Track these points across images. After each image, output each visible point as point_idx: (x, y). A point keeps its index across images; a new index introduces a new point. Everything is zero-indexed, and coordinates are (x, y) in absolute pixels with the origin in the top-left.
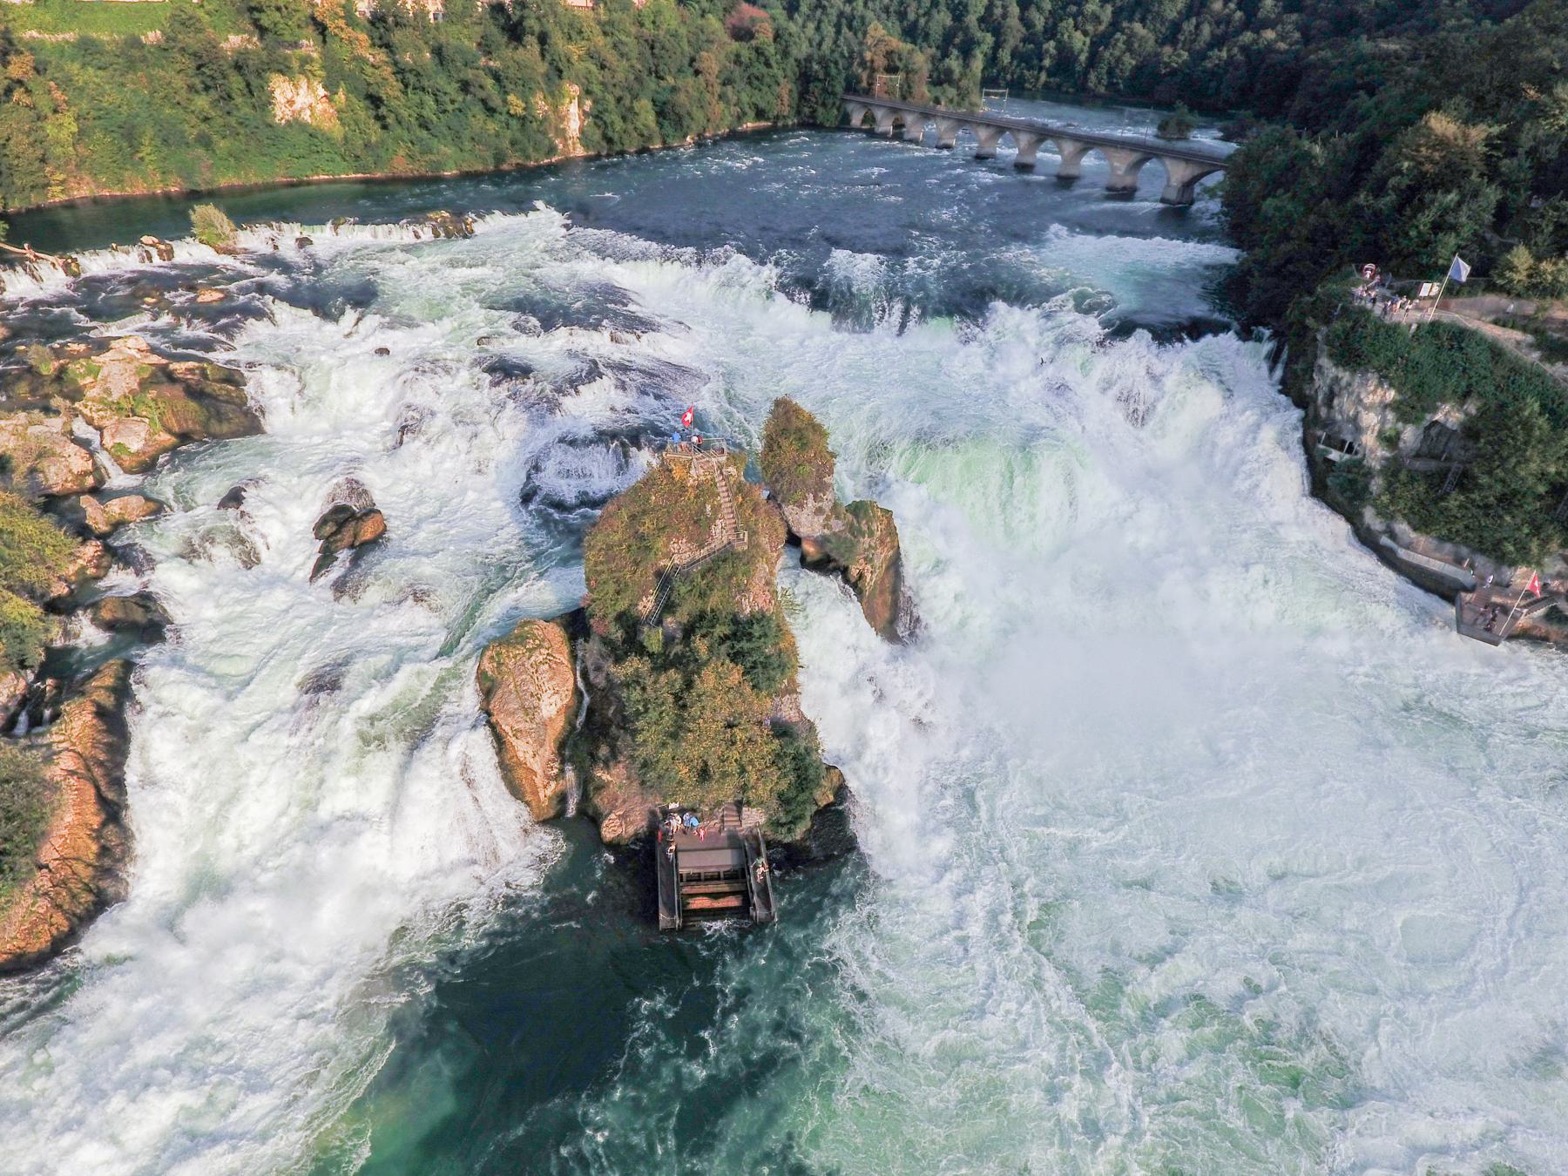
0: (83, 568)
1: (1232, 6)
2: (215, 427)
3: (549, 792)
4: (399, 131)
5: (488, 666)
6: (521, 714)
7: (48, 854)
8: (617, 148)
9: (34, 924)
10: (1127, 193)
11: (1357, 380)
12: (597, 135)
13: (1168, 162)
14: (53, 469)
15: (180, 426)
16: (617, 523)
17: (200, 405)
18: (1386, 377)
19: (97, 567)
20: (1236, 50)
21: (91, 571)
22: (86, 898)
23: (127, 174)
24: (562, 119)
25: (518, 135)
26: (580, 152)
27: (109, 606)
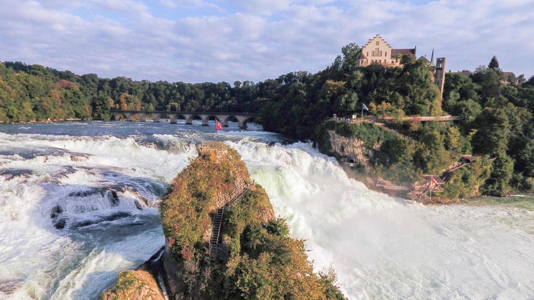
18: (360, 137)
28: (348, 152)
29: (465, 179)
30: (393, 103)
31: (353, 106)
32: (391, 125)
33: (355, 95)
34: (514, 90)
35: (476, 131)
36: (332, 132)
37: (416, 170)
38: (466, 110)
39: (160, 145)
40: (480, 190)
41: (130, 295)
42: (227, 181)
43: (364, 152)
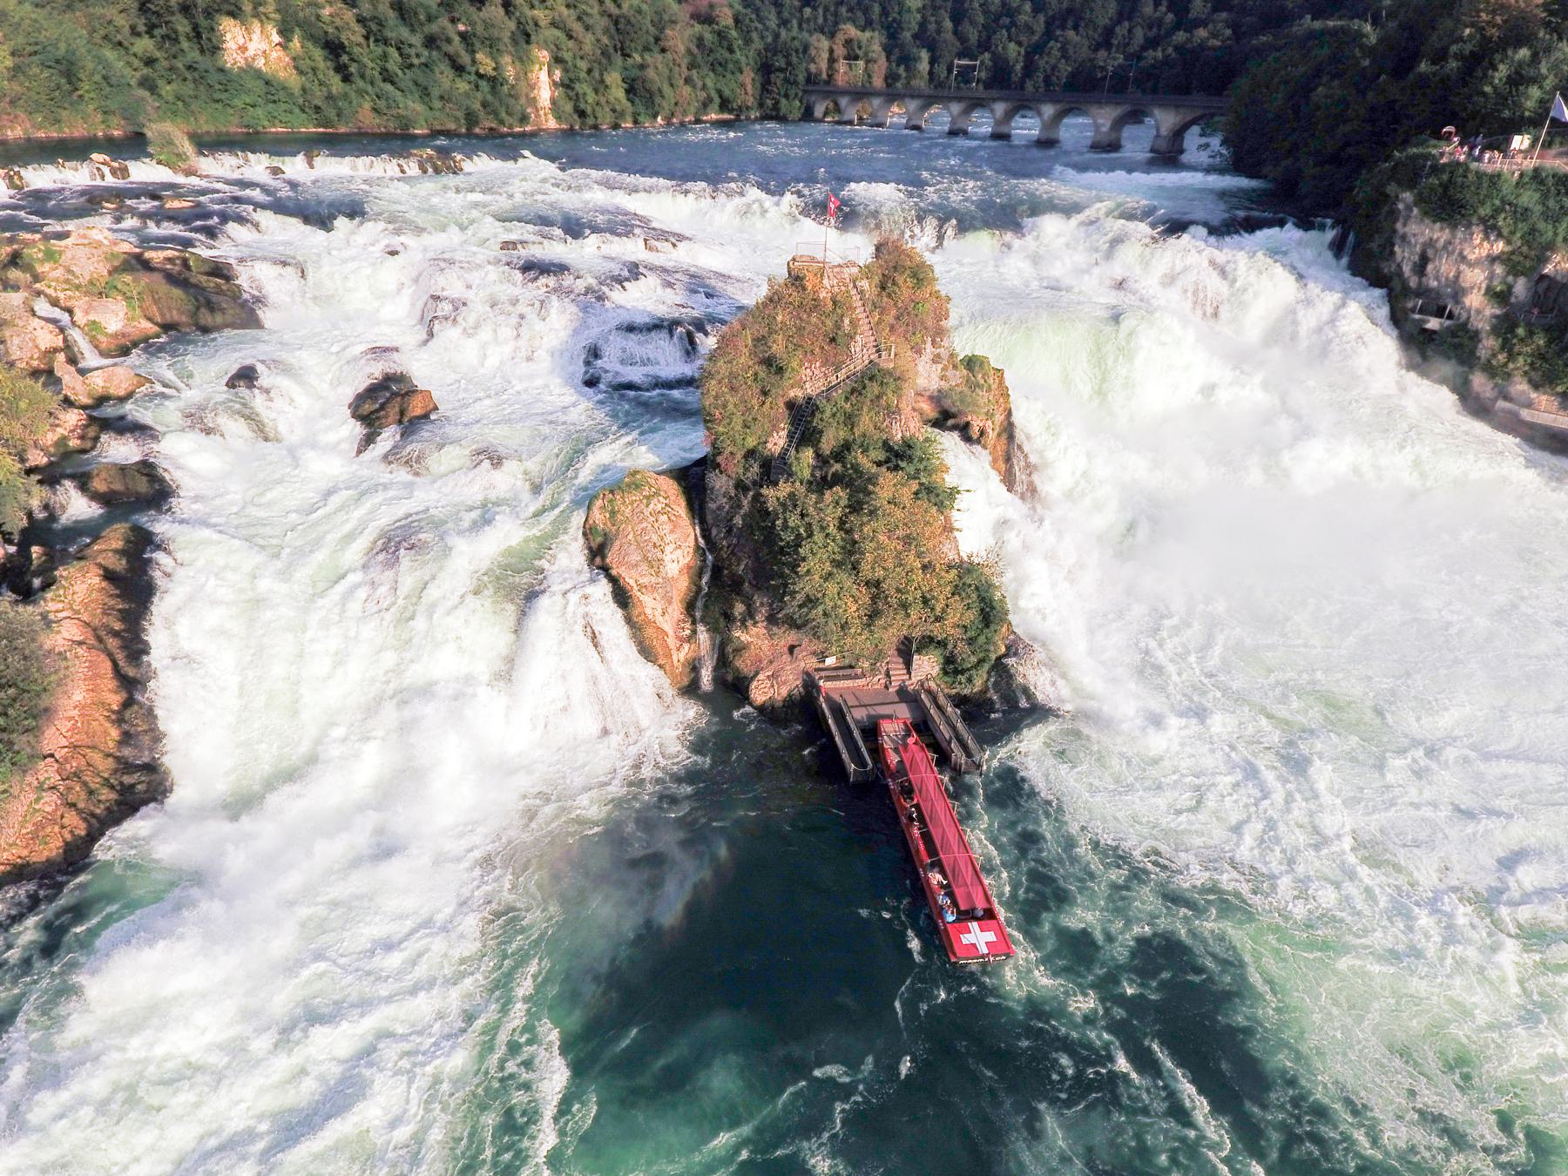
0: (64, 439)
1: (1163, 9)
2: (206, 318)
3: (682, 656)
4: (361, 84)
5: (598, 517)
6: (644, 566)
7: (54, 738)
8: (590, 121)
9: (40, 826)
11: (1460, 235)
12: (568, 107)
14: (16, 341)
15: (162, 315)
16: (741, 344)
17: (187, 293)
18: (1494, 227)
19: (82, 437)
20: (1170, 50)
21: (74, 443)
22: (107, 795)
23: (65, 114)
24: (532, 87)
25: (489, 98)
26: (552, 124)
27: (103, 475)
28: (1437, 278)
41: (632, 503)
42: (833, 340)
43: (1495, 283)
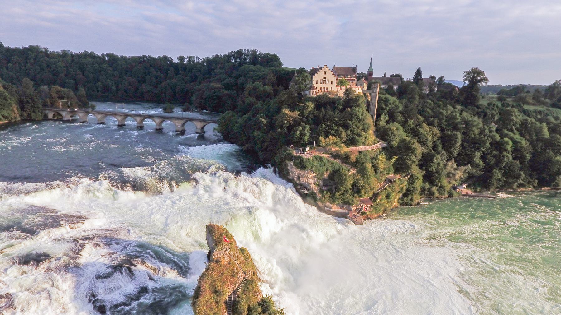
10: (182, 133)
13: (194, 122)
29: (388, 197)
30: (338, 137)
31: (306, 138)
32: (336, 156)
33: (308, 127)
34: (430, 104)
35: (397, 157)
36: (290, 164)
37: (353, 196)
38: (392, 133)
39: (138, 186)
40: (398, 202)
